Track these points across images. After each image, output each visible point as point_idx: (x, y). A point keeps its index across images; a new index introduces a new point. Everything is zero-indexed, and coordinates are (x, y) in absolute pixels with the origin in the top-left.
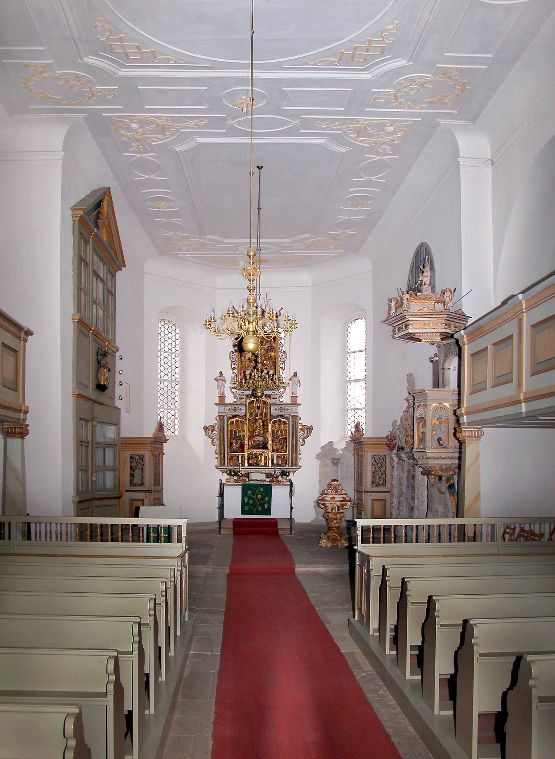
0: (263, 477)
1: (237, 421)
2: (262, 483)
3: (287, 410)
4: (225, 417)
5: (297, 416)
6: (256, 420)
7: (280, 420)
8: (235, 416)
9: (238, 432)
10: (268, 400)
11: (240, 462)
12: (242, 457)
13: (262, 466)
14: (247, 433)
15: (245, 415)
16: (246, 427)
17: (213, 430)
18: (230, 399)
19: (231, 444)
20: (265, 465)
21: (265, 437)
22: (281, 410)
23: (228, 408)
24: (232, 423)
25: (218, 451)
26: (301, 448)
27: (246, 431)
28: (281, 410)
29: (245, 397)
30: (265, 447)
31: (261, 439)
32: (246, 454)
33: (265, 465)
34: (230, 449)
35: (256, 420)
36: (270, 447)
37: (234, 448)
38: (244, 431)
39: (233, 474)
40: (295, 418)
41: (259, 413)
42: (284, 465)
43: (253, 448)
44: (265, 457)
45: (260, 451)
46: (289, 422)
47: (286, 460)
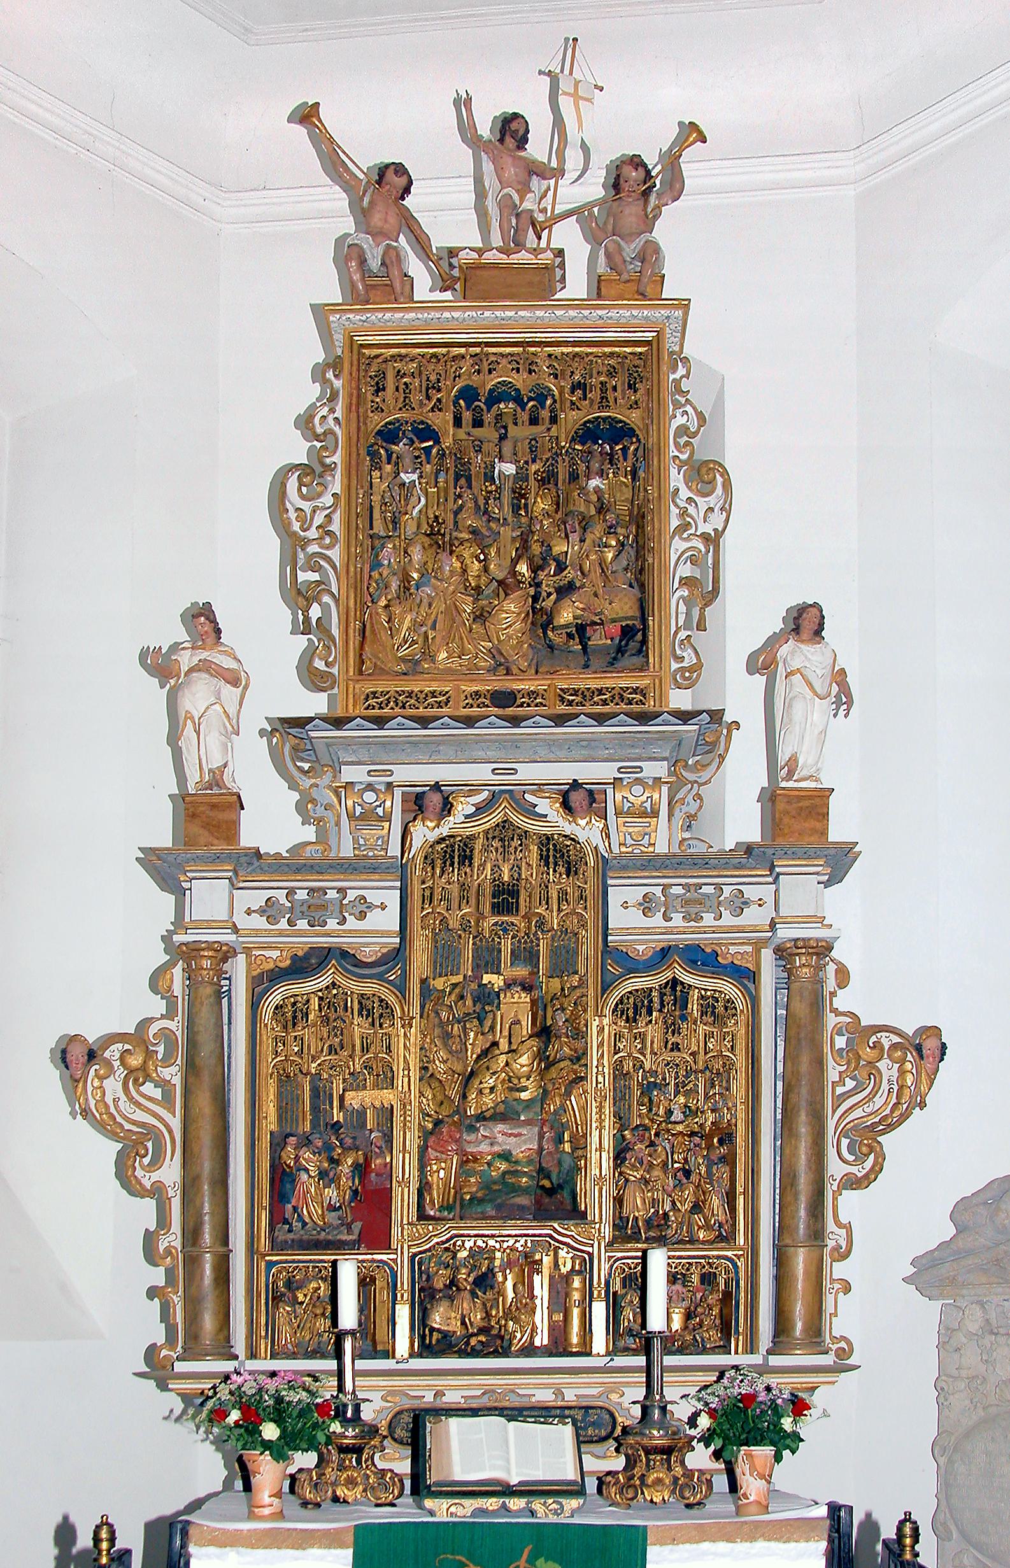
0: (549, 1453)
1: (330, 1002)
2: (544, 1511)
3: (740, 905)
4: (239, 971)
5: (822, 950)
6: (487, 998)
7: (679, 989)
8: (302, 966)
9: (338, 1087)
10: (586, 831)
11: (348, 1318)
12: (365, 1282)
13: (529, 1350)
14: (406, 1097)
15: (397, 956)
16: (407, 1044)
17: (137, 1076)
18: (272, 820)
19: (282, 1180)
20: (559, 1334)
21: (556, 1128)
22: (693, 906)
23: (257, 899)
24: (292, 1016)
25: (173, 1239)
26: (849, 1206)
27: (408, 1080)
28: (693, 906)
29: (396, 805)
30: (555, 1198)
31: (521, 1142)
32: (399, 1257)
33: (559, 1346)
34: (277, 1218)
35: (487, 998)
36: (597, 1199)
37: (313, 1212)
38: (387, 1079)
39: (270, 1431)
40: (808, 960)
41: (507, 946)
42: (713, 1336)
43: (460, 1207)
44: (560, 1286)
45: (507, 1238)
46: (755, 1002)
47: (727, 1296)
